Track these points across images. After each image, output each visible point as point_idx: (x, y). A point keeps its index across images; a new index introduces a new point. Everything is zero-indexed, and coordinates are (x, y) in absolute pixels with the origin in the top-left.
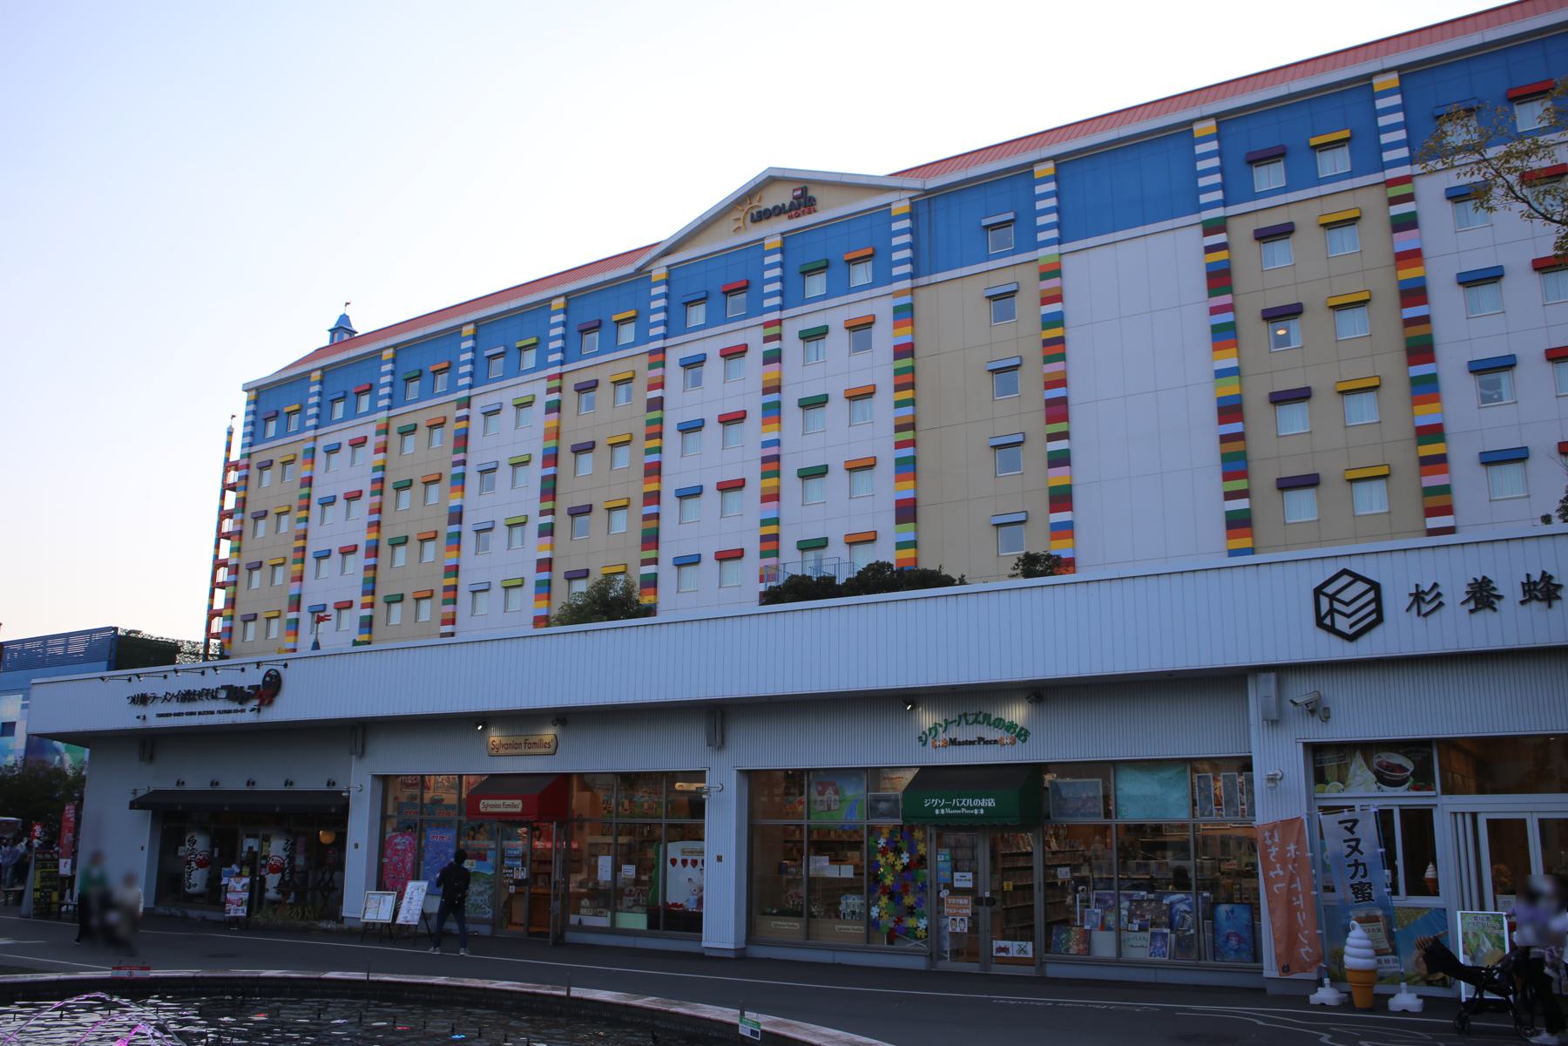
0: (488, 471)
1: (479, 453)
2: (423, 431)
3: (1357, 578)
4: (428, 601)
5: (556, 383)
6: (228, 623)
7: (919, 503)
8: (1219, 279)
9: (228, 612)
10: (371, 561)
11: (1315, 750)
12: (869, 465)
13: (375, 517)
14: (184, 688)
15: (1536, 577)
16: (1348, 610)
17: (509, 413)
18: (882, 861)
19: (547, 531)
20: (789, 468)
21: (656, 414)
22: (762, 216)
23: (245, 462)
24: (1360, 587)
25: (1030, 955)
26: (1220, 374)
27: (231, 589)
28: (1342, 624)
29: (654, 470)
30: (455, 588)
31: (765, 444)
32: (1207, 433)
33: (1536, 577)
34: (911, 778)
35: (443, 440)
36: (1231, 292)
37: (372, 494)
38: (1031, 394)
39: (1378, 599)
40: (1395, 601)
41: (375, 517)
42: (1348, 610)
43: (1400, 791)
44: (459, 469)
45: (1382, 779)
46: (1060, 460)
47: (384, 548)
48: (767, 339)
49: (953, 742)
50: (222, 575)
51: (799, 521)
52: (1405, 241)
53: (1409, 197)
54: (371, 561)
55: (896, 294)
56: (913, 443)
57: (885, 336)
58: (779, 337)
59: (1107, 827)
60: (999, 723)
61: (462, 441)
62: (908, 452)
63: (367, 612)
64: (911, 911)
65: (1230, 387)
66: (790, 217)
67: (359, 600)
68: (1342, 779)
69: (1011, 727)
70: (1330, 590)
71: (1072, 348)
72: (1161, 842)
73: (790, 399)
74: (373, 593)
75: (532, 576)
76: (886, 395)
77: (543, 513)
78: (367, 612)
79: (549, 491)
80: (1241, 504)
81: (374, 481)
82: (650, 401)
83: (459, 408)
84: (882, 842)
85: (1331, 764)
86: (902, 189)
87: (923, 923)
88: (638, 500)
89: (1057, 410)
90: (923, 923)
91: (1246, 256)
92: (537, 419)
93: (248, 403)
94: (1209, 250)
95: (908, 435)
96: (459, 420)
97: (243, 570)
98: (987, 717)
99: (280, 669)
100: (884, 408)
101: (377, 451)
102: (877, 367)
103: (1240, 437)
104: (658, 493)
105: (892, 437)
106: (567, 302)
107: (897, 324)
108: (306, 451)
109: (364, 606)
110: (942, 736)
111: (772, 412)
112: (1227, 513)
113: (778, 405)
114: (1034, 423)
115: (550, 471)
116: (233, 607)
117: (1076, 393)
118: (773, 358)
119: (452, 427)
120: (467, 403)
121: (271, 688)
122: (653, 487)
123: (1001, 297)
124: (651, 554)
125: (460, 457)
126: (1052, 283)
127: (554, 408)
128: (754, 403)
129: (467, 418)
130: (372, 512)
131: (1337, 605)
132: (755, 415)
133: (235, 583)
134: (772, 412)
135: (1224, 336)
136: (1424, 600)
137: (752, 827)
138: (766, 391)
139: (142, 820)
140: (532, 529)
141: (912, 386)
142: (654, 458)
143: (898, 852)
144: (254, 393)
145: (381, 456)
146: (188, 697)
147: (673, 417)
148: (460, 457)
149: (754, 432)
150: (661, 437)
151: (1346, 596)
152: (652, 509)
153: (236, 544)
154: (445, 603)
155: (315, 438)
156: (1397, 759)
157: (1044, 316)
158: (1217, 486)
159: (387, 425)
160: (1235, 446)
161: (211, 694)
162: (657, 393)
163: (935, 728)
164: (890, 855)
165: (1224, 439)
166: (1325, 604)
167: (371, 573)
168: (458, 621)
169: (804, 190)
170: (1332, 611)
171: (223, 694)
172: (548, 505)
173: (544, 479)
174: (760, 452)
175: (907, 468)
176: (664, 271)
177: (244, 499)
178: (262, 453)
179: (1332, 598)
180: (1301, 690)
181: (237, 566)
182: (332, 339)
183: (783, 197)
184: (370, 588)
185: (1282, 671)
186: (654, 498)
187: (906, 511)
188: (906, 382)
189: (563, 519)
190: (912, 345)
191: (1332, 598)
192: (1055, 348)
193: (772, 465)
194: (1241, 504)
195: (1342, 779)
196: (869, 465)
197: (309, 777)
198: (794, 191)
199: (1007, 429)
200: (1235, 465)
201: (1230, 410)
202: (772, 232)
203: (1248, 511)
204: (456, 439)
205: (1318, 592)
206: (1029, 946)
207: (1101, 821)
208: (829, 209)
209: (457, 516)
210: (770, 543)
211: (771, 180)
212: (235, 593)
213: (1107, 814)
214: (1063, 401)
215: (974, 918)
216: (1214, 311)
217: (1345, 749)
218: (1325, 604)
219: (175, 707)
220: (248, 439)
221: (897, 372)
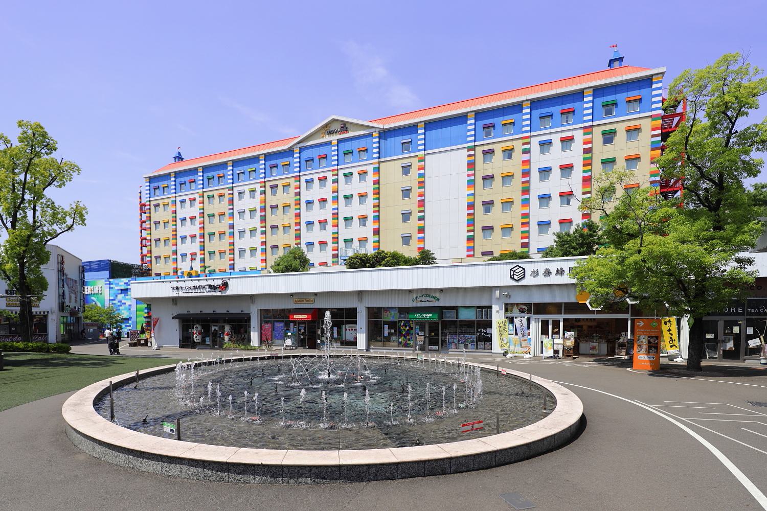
0: (242, 213)
3: (520, 267)
8: (471, 165)
9: (149, 255)
11: (506, 305)
15: (559, 269)
16: (517, 274)
18: (402, 328)
19: (264, 233)
22: (331, 133)
24: (521, 269)
28: (516, 277)
30: (233, 249)
33: (559, 269)
39: (524, 272)
40: (528, 273)
42: (517, 274)
46: (422, 219)
49: (421, 301)
54: (202, 240)
57: (371, 177)
59: (457, 321)
64: (409, 340)
66: (340, 134)
67: (198, 253)
70: (514, 270)
74: (204, 250)
76: (371, 196)
78: (203, 256)
79: (264, 220)
84: (402, 324)
85: (509, 308)
86: (377, 128)
87: (412, 342)
90: (412, 342)
96: (229, 194)
99: (228, 280)
100: (370, 200)
102: (368, 186)
105: (373, 209)
106: (265, 156)
107: (374, 173)
108: (172, 201)
110: (418, 300)
111: (336, 199)
114: (414, 208)
117: (427, 199)
119: (227, 197)
120: (232, 189)
121: (225, 285)
122: (298, 221)
125: (231, 207)
128: (330, 197)
131: (515, 273)
132: (330, 200)
134: (336, 199)
135: (471, 184)
136: (535, 273)
137: (368, 321)
139: (176, 322)
140: (259, 232)
143: (406, 327)
146: (194, 288)
150: (300, 204)
151: (517, 271)
155: (175, 197)
156: (524, 307)
157: (522, 243)
158: (466, 228)
161: (204, 288)
164: (404, 327)
165: (468, 215)
166: (512, 273)
167: (202, 244)
169: (345, 125)
170: (514, 274)
172: (264, 225)
173: (261, 216)
175: (377, 219)
179: (514, 271)
181: (150, 240)
187: (377, 232)
188: (377, 192)
189: (269, 230)
191: (514, 271)
192: (422, 184)
197: (235, 310)
198: (342, 124)
200: (471, 223)
201: (471, 206)
202: (334, 138)
204: (229, 201)
205: (511, 270)
206: (437, 347)
207: (455, 319)
209: (232, 226)
213: (457, 318)
214: (424, 201)
215: (424, 342)
217: (512, 304)
218: (512, 273)
221: (374, 189)
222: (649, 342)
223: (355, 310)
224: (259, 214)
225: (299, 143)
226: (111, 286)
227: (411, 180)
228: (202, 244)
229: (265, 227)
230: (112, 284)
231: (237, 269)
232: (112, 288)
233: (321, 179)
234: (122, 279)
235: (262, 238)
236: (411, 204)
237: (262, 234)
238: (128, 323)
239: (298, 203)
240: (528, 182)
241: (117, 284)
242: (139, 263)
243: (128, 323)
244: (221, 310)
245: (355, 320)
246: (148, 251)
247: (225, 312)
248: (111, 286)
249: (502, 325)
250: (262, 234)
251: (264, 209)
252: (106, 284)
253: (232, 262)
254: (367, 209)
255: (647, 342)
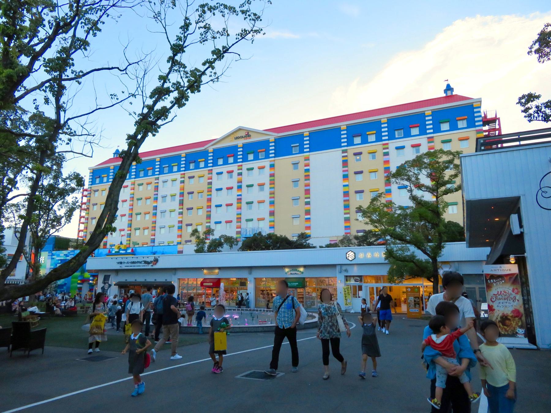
0: (164, 197)
1: (161, 192)
2: (145, 185)
4: (147, 230)
5: (183, 176)
6: (85, 234)
7: (275, 212)
8: (345, 163)
9: (85, 231)
10: (130, 219)
11: (346, 276)
12: (263, 202)
13: (131, 207)
14: (132, 261)
17: (170, 183)
20: (244, 202)
21: (210, 186)
22: (237, 138)
23: (90, 189)
25: (396, 132)
26: (344, 186)
27: (86, 224)
29: (209, 200)
31: (238, 195)
32: (341, 198)
34: (513, 361)
35: (151, 188)
36: (347, 167)
37: (130, 201)
38: (301, 189)
41: (131, 207)
43: (358, 283)
44: (156, 196)
45: (355, 281)
46: (308, 203)
47: (134, 215)
48: (238, 170)
49: (291, 274)
50: (83, 220)
51: (246, 213)
52: (386, 158)
53: (387, 148)
54: (130, 219)
55: (271, 161)
56: (274, 197)
58: (241, 169)
60: (298, 271)
61: (157, 188)
62: (273, 199)
63: (129, 232)
65: (346, 189)
68: (350, 281)
69: (301, 271)
71: (311, 178)
72: (480, 291)
73: (244, 185)
75: (177, 225)
77: (180, 209)
78: (129, 232)
79: (181, 203)
80: (348, 216)
81: (131, 197)
82: (208, 182)
83: (156, 180)
88: (205, 207)
89: (307, 192)
91: (351, 159)
92: (178, 185)
93: (90, 173)
94: (343, 157)
95: (273, 196)
96: (155, 183)
97: (90, 219)
98: (297, 270)
101: (131, 190)
102: (266, 179)
103: (348, 200)
104: (211, 206)
105: (269, 196)
109: (128, 230)
111: (240, 188)
112: (345, 218)
113: (241, 186)
115: (182, 198)
116: (87, 229)
118: (240, 174)
119: (153, 185)
121: (156, 261)
122: (209, 204)
123: (295, 164)
124: (209, 221)
125: (156, 193)
126: (307, 162)
127: (182, 182)
128: (235, 185)
129: (158, 183)
130: (130, 206)
133: (87, 223)
134: (240, 188)
135: (345, 177)
138: (238, 182)
141: (274, 184)
142: (209, 197)
144: (92, 170)
145: (133, 191)
146: (133, 263)
147: (214, 187)
148: (156, 193)
149: (235, 191)
151: (350, 254)
152: (209, 209)
153: (87, 212)
154: (152, 230)
156: (357, 278)
159: (134, 183)
160: (347, 203)
161: (141, 262)
162: (210, 181)
163: (288, 272)
167: (130, 222)
168: (156, 235)
169: (248, 133)
171: (143, 262)
173: (180, 200)
174: (236, 197)
175: (272, 203)
176: (212, 149)
177: (90, 200)
178: (95, 187)
180: (344, 268)
182: (114, 156)
183: (243, 134)
184: (130, 226)
185: (341, 265)
186: (209, 207)
187: (272, 213)
188: (272, 183)
189: (185, 211)
190: (274, 174)
192: (307, 177)
193: (239, 200)
194: (348, 216)
195: (350, 281)
196: (263, 202)
197: (161, 278)
199: (296, 196)
201: (346, 194)
203: (349, 217)
208: (254, 139)
209: (155, 208)
210: (239, 219)
211: (240, 129)
212: (87, 225)
216: (344, 171)
217: (350, 276)
219: (130, 265)
220: (90, 183)
222: (415, 301)
223: (246, 279)
224: (178, 198)
225: (212, 145)
226: (53, 257)
227: (300, 173)
228: (130, 222)
229: (182, 209)
230: (54, 255)
231: (156, 244)
232: (53, 258)
233: (229, 172)
234: (63, 252)
235: (179, 218)
236: (300, 191)
237: (179, 214)
238: (63, 288)
239: (210, 190)
240: (348, 200)
241: (58, 256)
242: (76, 238)
243: (63, 288)
244: (150, 278)
245: (439, 291)
246: (84, 228)
247: (144, 281)
248: (53, 257)
249: (346, 290)
250: (179, 214)
251: (182, 195)
252: (49, 255)
253: (153, 237)
254: (265, 195)
255: (413, 301)
